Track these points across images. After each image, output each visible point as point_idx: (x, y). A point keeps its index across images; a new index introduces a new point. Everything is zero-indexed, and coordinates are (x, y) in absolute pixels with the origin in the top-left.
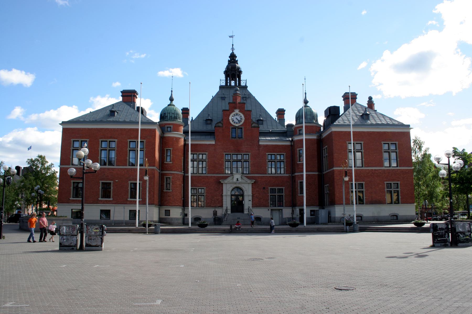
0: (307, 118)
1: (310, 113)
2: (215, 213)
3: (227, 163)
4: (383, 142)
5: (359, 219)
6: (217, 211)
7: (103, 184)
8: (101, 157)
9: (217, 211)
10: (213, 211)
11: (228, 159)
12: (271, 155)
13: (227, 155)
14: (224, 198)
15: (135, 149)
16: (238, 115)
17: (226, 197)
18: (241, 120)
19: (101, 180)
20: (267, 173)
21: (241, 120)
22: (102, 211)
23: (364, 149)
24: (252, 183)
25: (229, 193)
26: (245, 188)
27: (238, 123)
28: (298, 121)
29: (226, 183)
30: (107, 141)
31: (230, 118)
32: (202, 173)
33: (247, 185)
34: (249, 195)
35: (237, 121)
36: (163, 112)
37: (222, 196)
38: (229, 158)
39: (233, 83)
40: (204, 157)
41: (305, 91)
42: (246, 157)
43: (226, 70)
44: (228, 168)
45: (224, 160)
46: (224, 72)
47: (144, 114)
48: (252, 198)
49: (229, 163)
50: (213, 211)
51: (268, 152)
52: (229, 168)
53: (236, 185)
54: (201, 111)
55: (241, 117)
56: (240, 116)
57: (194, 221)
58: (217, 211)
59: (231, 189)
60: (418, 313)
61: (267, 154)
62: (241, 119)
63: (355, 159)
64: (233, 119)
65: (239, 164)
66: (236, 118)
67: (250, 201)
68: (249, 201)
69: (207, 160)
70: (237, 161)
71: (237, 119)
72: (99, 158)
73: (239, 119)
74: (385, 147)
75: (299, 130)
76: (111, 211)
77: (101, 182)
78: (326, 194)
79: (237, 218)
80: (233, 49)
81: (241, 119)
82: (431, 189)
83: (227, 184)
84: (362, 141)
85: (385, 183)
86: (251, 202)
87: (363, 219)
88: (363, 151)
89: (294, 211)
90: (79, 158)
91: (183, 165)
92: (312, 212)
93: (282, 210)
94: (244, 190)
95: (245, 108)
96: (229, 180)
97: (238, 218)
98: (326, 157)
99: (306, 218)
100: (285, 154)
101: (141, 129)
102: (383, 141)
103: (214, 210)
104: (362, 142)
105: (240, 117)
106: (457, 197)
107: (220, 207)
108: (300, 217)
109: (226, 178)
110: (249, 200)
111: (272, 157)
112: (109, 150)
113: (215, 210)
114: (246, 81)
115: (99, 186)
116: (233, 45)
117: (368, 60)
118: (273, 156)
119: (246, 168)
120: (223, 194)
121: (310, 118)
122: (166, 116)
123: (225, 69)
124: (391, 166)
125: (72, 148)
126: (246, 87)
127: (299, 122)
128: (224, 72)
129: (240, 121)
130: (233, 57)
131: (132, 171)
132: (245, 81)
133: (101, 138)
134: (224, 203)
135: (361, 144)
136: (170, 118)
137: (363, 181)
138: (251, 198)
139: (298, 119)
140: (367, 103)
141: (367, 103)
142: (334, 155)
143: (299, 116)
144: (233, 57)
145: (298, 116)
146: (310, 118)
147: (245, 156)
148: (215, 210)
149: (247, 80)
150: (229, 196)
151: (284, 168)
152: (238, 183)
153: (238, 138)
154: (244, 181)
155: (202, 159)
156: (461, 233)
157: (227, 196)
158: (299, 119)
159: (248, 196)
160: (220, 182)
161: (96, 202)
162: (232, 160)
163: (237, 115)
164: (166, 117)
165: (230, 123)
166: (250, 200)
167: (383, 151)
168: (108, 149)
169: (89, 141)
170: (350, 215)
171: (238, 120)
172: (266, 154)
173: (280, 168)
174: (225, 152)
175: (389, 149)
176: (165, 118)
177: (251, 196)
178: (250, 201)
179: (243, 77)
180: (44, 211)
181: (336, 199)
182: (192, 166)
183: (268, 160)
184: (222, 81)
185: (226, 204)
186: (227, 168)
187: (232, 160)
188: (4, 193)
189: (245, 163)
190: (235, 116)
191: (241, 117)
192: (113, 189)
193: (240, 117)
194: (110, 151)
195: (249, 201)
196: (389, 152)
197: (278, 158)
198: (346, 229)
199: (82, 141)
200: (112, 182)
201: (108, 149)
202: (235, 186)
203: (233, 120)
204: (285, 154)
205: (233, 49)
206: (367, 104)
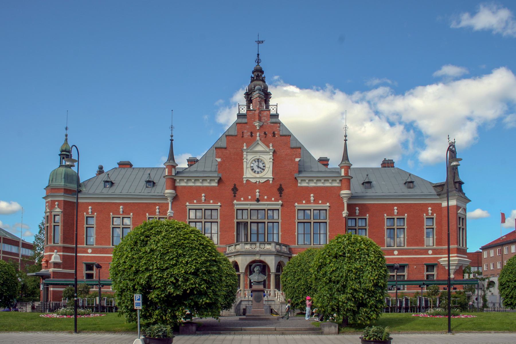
8: (433, 237)
23: (281, 219)
30: (120, 217)
55: (264, 163)
60: (55, 343)
72: (435, 237)
95: (74, 202)
106: (141, 272)
112: (123, 228)
114: (277, 106)
125: (112, 226)
126: (276, 116)
132: (275, 106)
168: (121, 226)
181: (30, 255)
184: (271, 106)
188: (249, 321)
190: (263, 164)
194: (114, 229)
197: (324, 237)
199: (123, 218)
201: (121, 226)
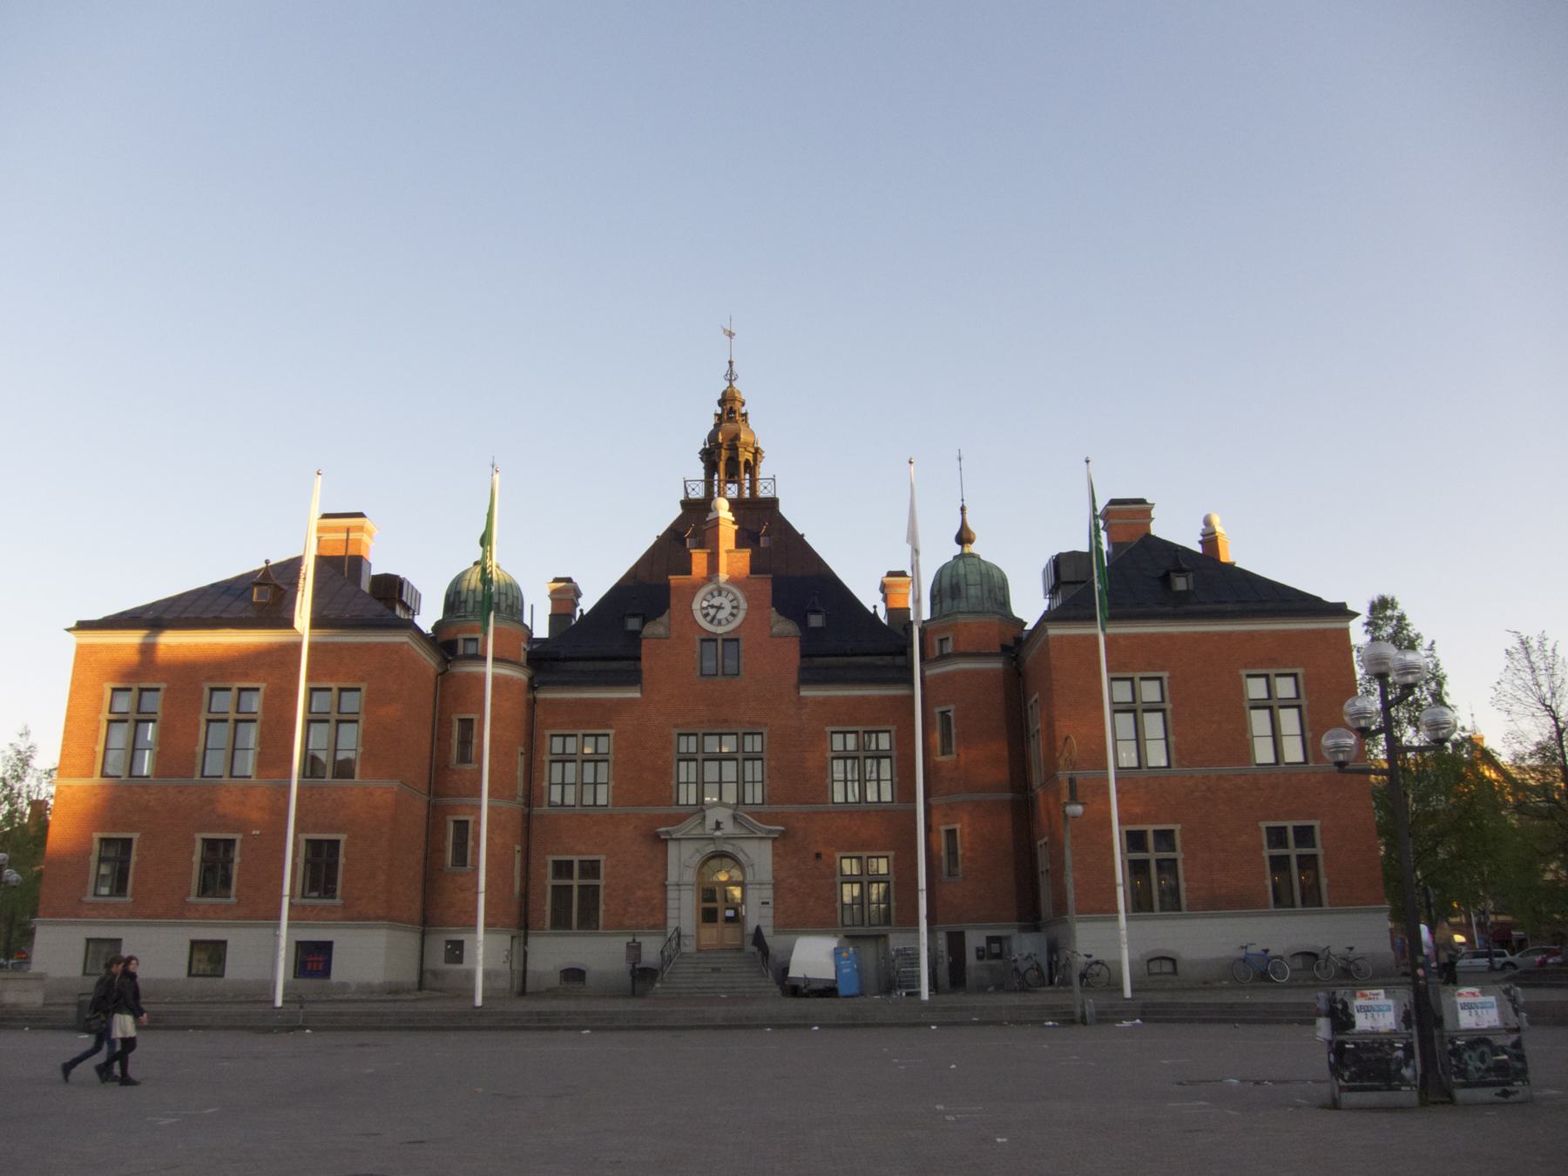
0: (967, 598)
1: (978, 579)
2: (634, 950)
3: (683, 765)
4: (1243, 672)
5: (1164, 970)
6: (640, 944)
7: (103, 844)
9: (643, 945)
10: (628, 943)
11: (688, 753)
12: (845, 733)
14: (672, 894)
15: (355, 718)
16: (724, 593)
17: (679, 890)
19: (200, 830)
20: (830, 800)
22: (195, 945)
23: (1171, 701)
24: (774, 839)
25: (690, 876)
26: (746, 854)
28: (937, 607)
29: (679, 839)
31: (696, 606)
32: (563, 804)
33: (755, 843)
34: (760, 884)
36: (454, 587)
37: (666, 886)
38: (693, 749)
39: (729, 489)
40: (604, 746)
41: (963, 500)
42: (754, 744)
43: (707, 446)
44: (753, 782)
45: (204, 716)
46: (700, 453)
47: (404, 599)
48: (775, 894)
49: (693, 765)
50: (628, 943)
51: (832, 724)
52: (756, 784)
53: (712, 846)
54: (609, 588)
57: (561, 983)
58: (640, 944)
59: (697, 858)
61: (829, 729)
63: (1141, 737)
65: (730, 769)
67: (767, 903)
68: (763, 903)
69: (611, 757)
70: (720, 758)
74: (1256, 689)
75: (941, 641)
76: (335, 946)
77: (199, 837)
78: (1043, 872)
79: (710, 970)
80: (731, 377)
83: (683, 842)
84: (1163, 669)
85: (1260, 828)
86: (769, 911)
87: (1179, 968)
88: (1168, 706)
89: (660, 950)
91: (520, 773)
92: (993, 945)
93: (885, 936)
94: (745, 866)
96: (689, 827)
97: (713, 969)
99: (1131, 963)
100: (893, 728)
102: (1246, 666)
103: (630, 939)
104: (1165, 675)
105: (731, 601)
107: (654, 927)
108: (950, 963)
109: (679, 819)
110: (764, 900)
111: (842, 743)
112: (237, 721)
113: (634, 940)
114: (774, 480)
115: (192, 853)
116: (730, 363)
118: (851, 739)
119: (753, 782)
120: (666, 879)
121: (980, 594)
122: (461, 602)
123: (705, 444)
124: (1280, 759)
127: (941, 612)
128: (700, 453)
130: (729, 407)
131: (313, 794)
133: (210, 679)
134: (671, 913)
135: (1160, 679)
136: (474, 608)
137: (1176, 822)
138: (768, 894)
139: (938, 598)
140: (1201, 538)
141: (1201, 538)
142: (1057, 723)
143: (940, 590)
144: (729, 407)
145: (935, 593)
146: (977, 597)
147: (748, 739)
148: (634, 940)
149: (776, 478)
150: (768, 886)
151: (891, 780)
152: (718, 838)
153: (724, 674)
154: (744, 831)
155: (564, 753)
157: (682, 888)
158: (941, 602)
159: (758, 886)
160: (657, 836)
161: (177, 913)
162: (700, 757)
164: (463, 605)
165: (696, 622)
166: (767, 900)
167: (1247, 705)
168: (233, 716)
169: (167, 690)
170: (1351, 949)
172: (825, 732)
173: (879, 780)
174: (676, 726)
175: (1270, 697)
176: (459, 608)
177: (771, 886)
178: (767, 903)
179: (764, 470)
182: (238, 753)
183: (833, 754)
185: (679, 918)
186: (751, 784)
187: (700, 757)
189: (748, 764)
192: (1328, 885)
195: (763, 903)
196: (1270, 708)
198: (1083, 1013)
200: (238, 837)
201: (233, 716)
202: (711, 848)
204: (893, 728)
205: (731, 377)
206: (1200, 542)
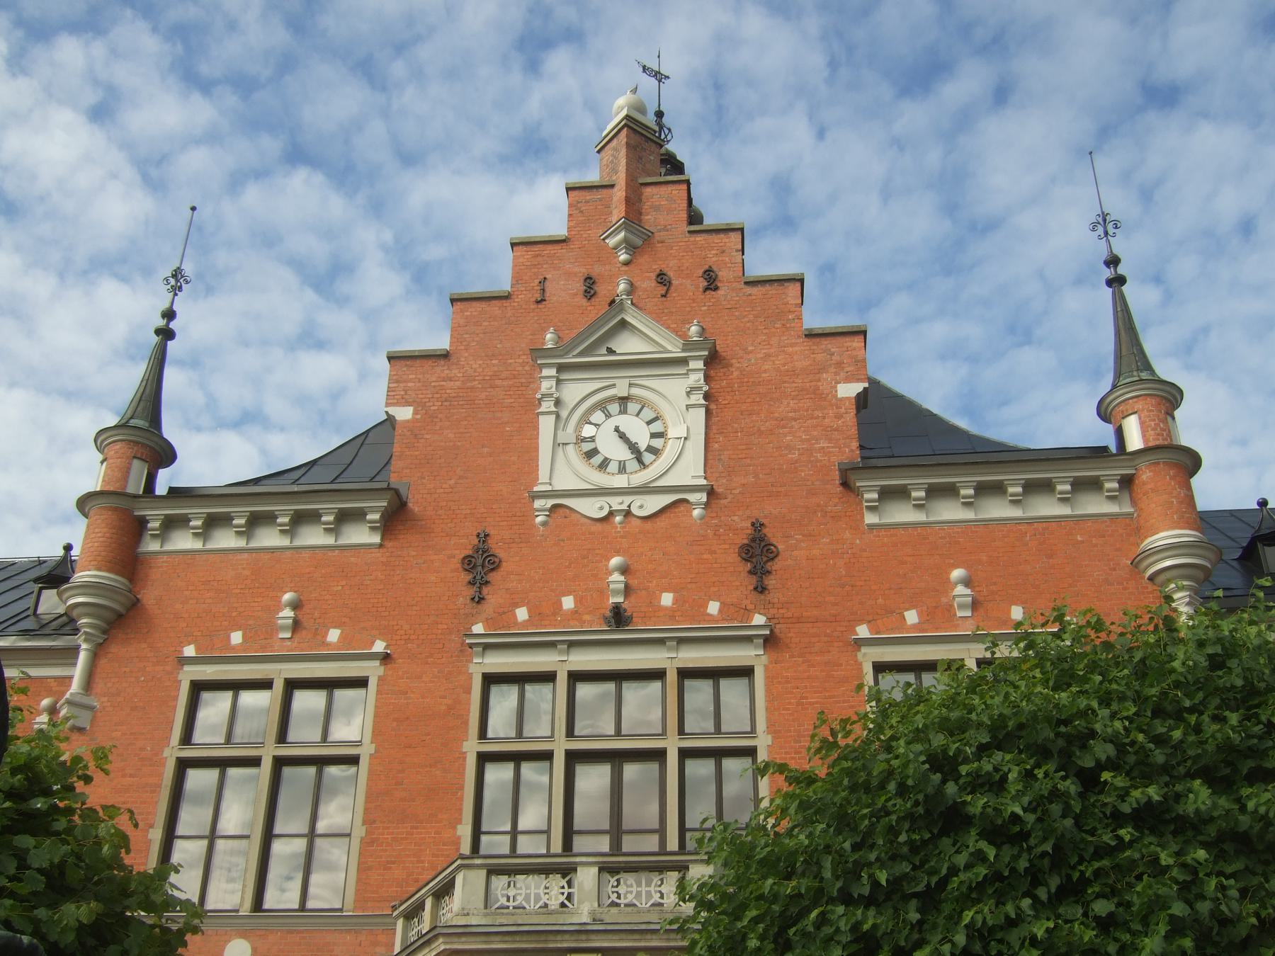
13: (705, 686)
18: (657, 443)
21: (657, 443)
27: (632, 465)
35: (623, 453)
55: (656, 419)
56: (653, 415)
62: (654, 435)
64: (592, 439)
66: (617, 429)
71: (622, 436)
73: (643, 441)
81: (654, 435)
82: (879, 739)
90: (770, 532)
98: (868, 453)
101: (75, 664)
105: (649, 423)
117: (957, 573)
129: (651, 449)
156: (905, 692)
163: (623, 411)
171: (633, 448)
180: (703, 940)
191: (656, 419)
193: (649, 423)
203: (587, 447)
